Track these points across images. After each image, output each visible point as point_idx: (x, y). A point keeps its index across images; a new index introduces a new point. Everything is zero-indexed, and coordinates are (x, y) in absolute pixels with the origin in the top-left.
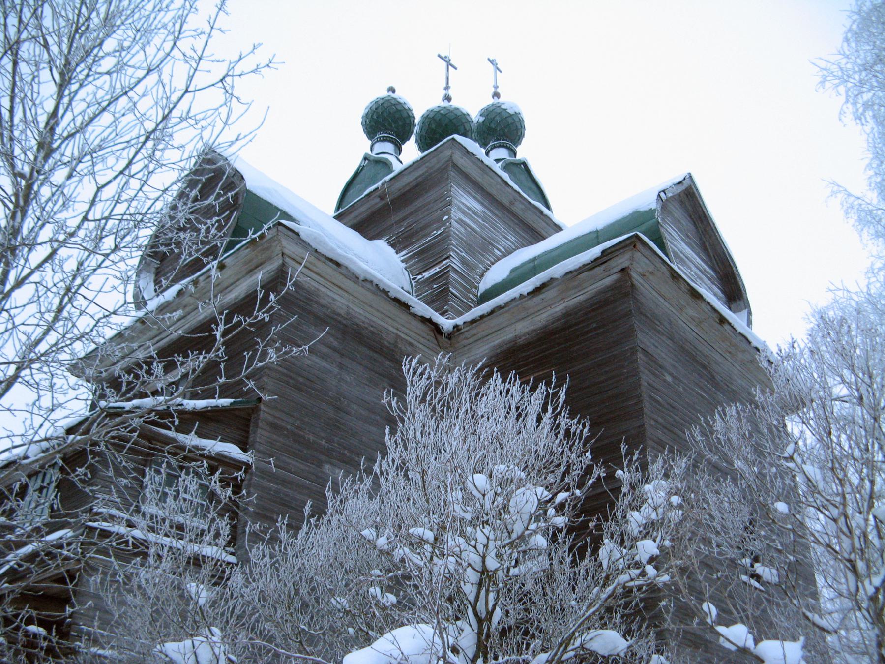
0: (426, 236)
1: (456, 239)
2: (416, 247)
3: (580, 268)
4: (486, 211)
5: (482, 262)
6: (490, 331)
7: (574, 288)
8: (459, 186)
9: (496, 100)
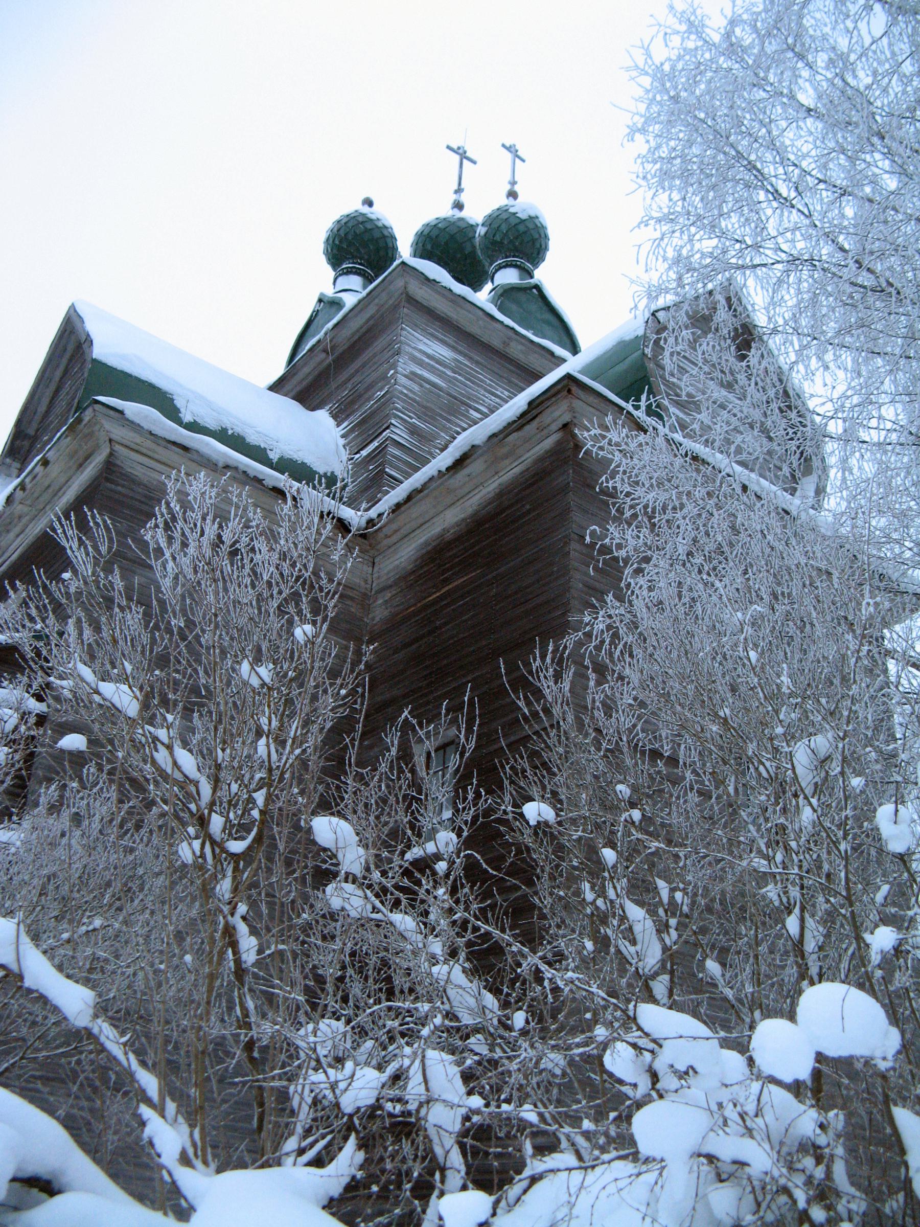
0: (368, 400)
1: (404, 401)
2: (356, 418)
3: (505, 427)
4: (461, 358)
5: (445, 429)
6: (414, 524)
7: (506, 456)
8: (415, 326)
9: (511, 201)
